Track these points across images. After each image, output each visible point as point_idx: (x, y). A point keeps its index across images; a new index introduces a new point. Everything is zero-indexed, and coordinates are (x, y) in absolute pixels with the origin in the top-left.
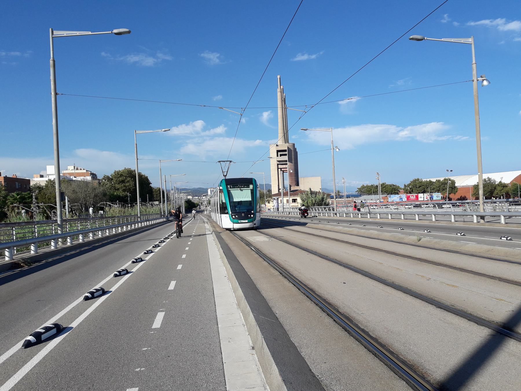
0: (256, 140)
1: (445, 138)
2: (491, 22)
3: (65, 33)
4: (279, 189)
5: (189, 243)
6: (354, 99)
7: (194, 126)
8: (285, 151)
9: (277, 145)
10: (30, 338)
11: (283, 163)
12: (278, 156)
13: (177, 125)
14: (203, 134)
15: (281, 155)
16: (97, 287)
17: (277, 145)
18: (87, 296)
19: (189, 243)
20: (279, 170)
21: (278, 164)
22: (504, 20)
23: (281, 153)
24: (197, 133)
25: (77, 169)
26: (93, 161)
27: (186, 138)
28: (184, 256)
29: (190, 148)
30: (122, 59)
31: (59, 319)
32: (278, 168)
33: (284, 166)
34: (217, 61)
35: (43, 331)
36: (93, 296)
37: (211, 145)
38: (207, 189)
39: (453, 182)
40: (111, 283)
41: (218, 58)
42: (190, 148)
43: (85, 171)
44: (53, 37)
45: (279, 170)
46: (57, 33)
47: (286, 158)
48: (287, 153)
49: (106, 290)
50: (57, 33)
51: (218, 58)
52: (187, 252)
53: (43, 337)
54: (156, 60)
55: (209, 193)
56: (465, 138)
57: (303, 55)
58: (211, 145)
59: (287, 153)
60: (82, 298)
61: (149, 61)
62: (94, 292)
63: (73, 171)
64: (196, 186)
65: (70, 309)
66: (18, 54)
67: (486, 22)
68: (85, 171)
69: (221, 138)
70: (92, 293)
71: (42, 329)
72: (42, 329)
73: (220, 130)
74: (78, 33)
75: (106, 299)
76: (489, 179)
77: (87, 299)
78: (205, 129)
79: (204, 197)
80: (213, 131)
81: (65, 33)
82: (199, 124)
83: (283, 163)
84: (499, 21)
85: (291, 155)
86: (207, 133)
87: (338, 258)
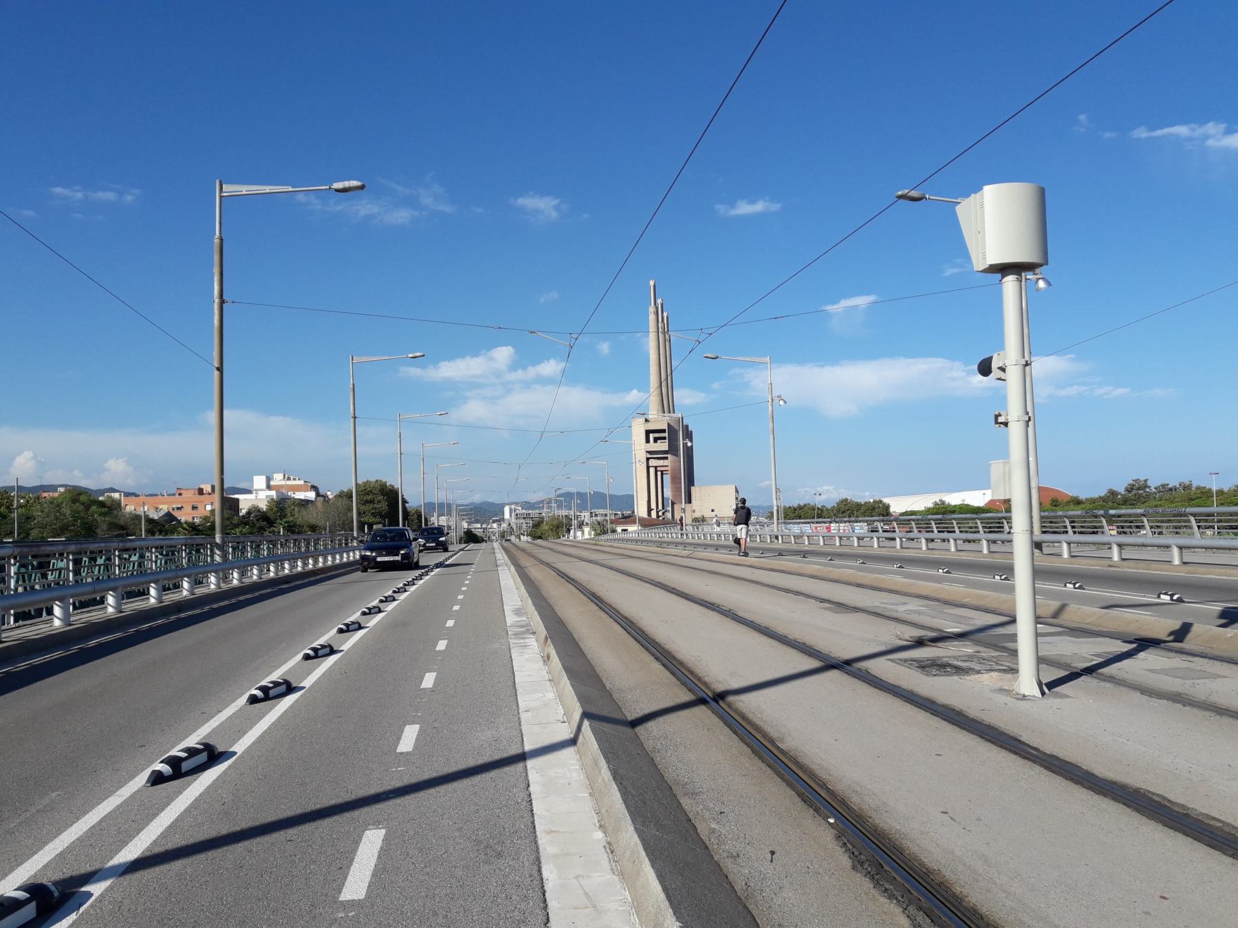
0: (628, 389)
1: (1073, 391)
2: (1193, 130)
3: (245, 189)
4: (650, 510)
5: (456, 608)
6: (862, 301)
7: (491, 359)
8: (664, 431)
9: (647, 420)
10: (160, 767)
11: (661, 455)
12: (648, 441)
13: (450, 357)
14: (512, 377)
15: (656, 440)
16: (192, 741)
17: (647, 420)
18: (159, 772)
19: (456, 608)
20: (652, 470)
21: (648, 459)
22: (1223, 126)
23: (657, 435)
24: (498, 374)
25: (289, 479)
26: (284, 453)
27: (473, 385)
28: (442, 645)
29: (475, 410)
30: (340, 208)
31: (209, 735)
32: (648, 467)
33: (661, 462)
34: (554, 214)
35: (184, 755)
36: (179, 770)
37: (522, 403)
38: (503, 505)
39: (888, 507)
40: (238, 726)
41: (556, 208)
42: (475, 410)
43: (302, 482)
44: (221, 197)
45: (652, 470)
46: (229, 189)
47: (663, 446)
48: (666, 435)
49: (221, 750)
50: (229, 189)
51: (556, 208)
52: (449, 634)
53: (185, 766)
54: (417, 213)
55: (507, 516)
56: (1121, 391)
57: (752, 202)
58: (522, 403)
59: (666, 435)
60: (143, 778)
61: (402, 216)
62: (181, 760)
63: (283, 483)
64: (477, 498)
65: (27, 865)
66: (111, 196)
67: (1182, 130)
68: (302, 482)
69: (549, 388)
70: (174, 762)
71: (182, 751)
72: (182, 751)
73: (550, 368)
74: (268, 189)
75: (225, 772)
76: (943, 502)
77: (157, 779)
78: (514, 366)
79: (495, 525)
80: (532, 371)
81: (245, 189)
82: (503, 354)
83: (661, 455)
84: (1211, 128)
85: (674, 441)
86: (520, 374)
87: (1067, 753)
